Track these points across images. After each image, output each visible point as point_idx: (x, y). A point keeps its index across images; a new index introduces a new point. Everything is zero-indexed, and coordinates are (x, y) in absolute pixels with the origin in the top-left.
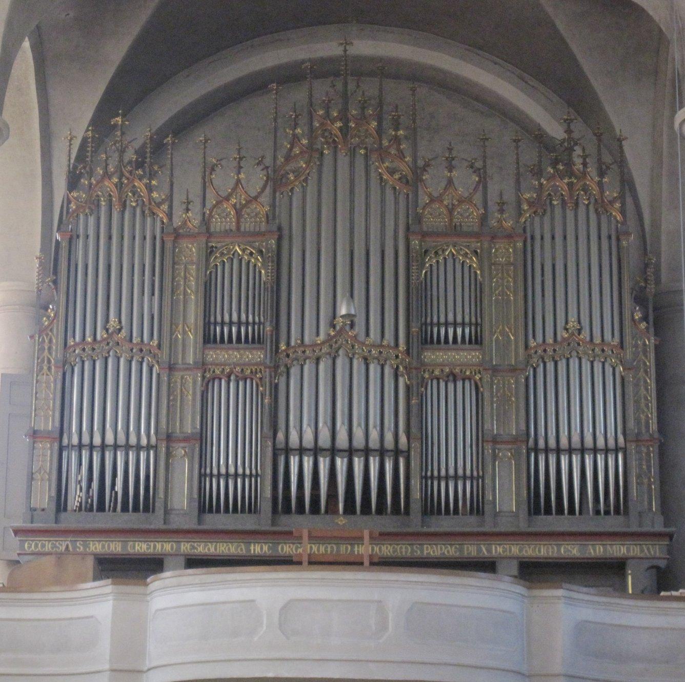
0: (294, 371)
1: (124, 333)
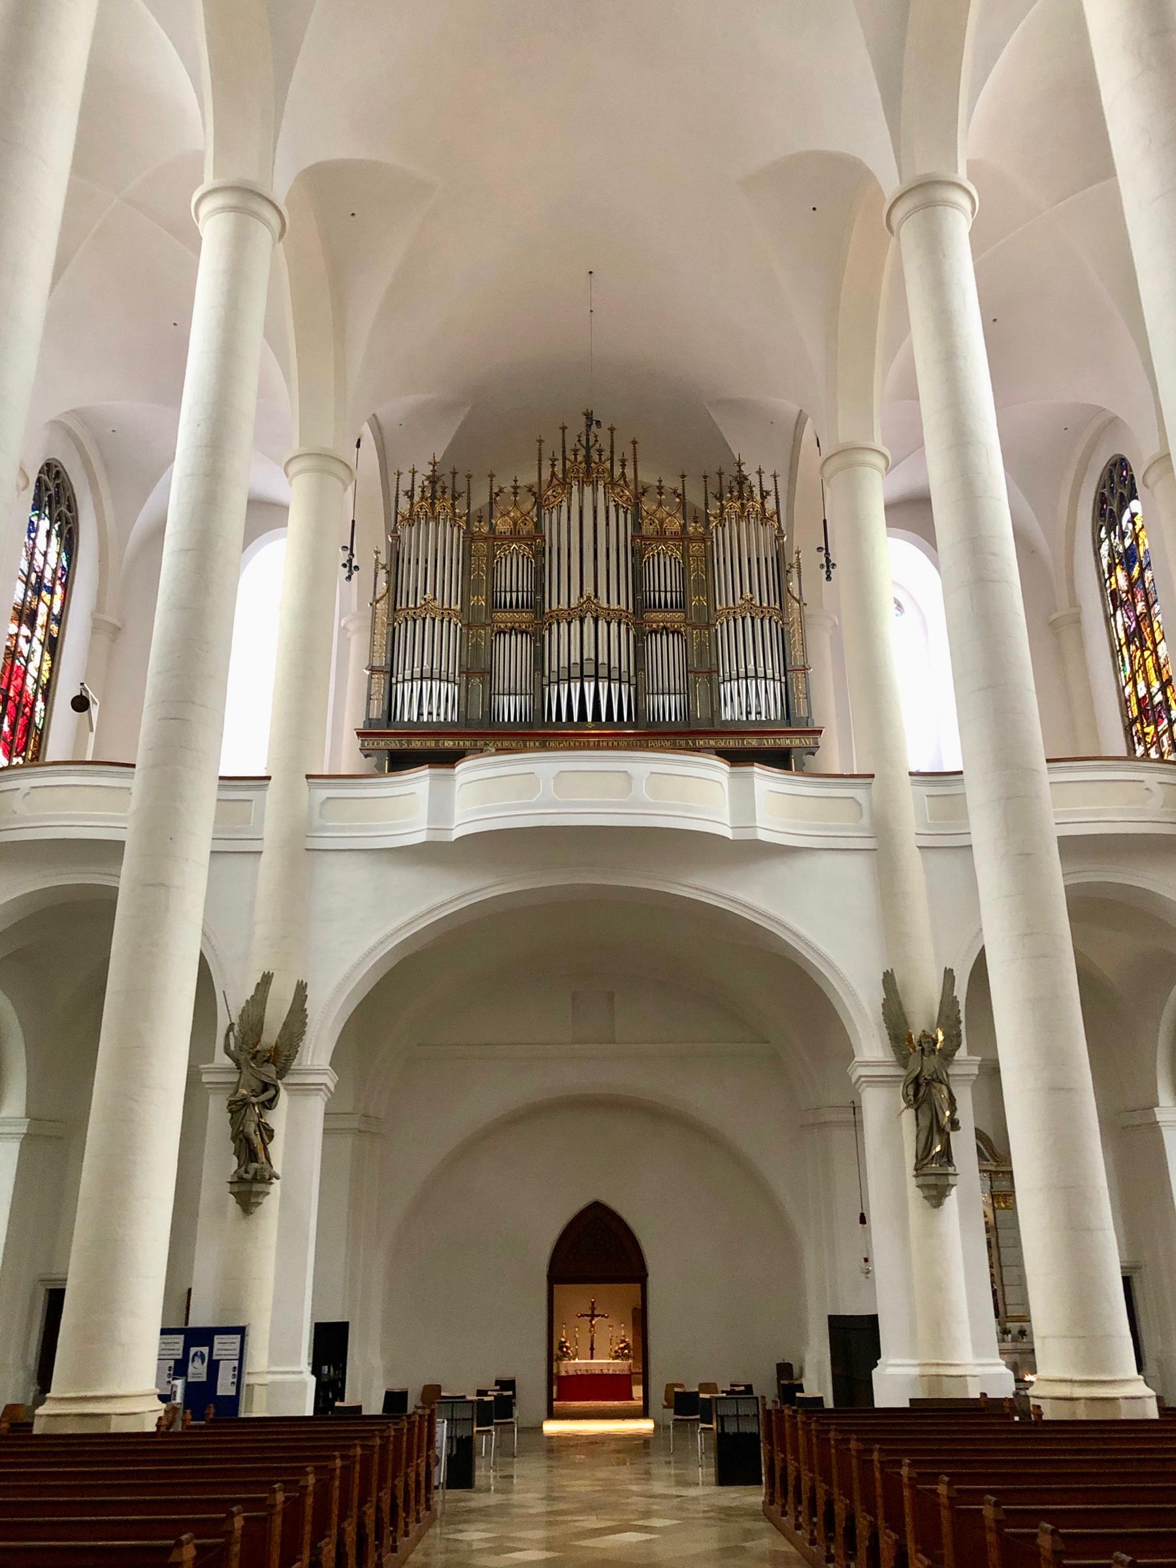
0: (555, 627)
1: (438, 603)
